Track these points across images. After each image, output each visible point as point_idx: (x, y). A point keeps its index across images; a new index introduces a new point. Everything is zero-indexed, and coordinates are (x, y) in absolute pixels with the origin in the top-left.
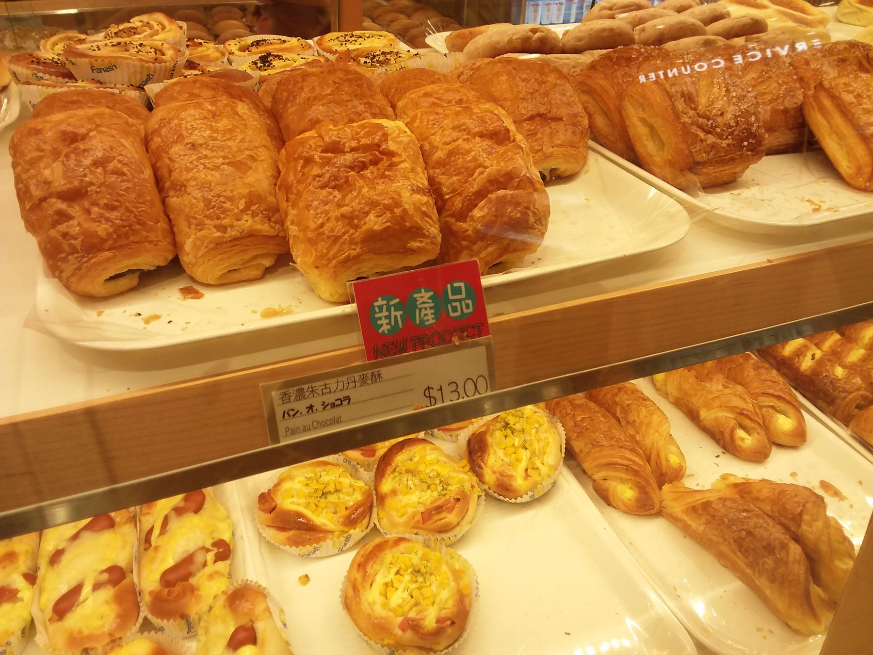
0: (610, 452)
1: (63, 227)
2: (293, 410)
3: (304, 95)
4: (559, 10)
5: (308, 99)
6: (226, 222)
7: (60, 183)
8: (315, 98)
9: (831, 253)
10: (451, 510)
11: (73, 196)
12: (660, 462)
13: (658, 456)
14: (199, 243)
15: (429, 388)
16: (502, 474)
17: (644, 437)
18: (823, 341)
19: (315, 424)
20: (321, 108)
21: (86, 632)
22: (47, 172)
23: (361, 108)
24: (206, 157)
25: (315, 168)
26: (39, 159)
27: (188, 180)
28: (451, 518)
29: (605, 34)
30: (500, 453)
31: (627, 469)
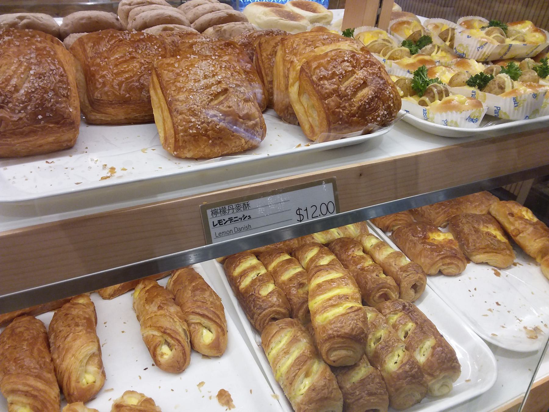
0: (15, 380)
2: (224, 220)
12: (70, 384)
13: (69, 378)
15: (299, 209)
17: (63, 360)
18: (270, 263)
19: (236, 230)
29: (84, 21)
31: (26, 394)
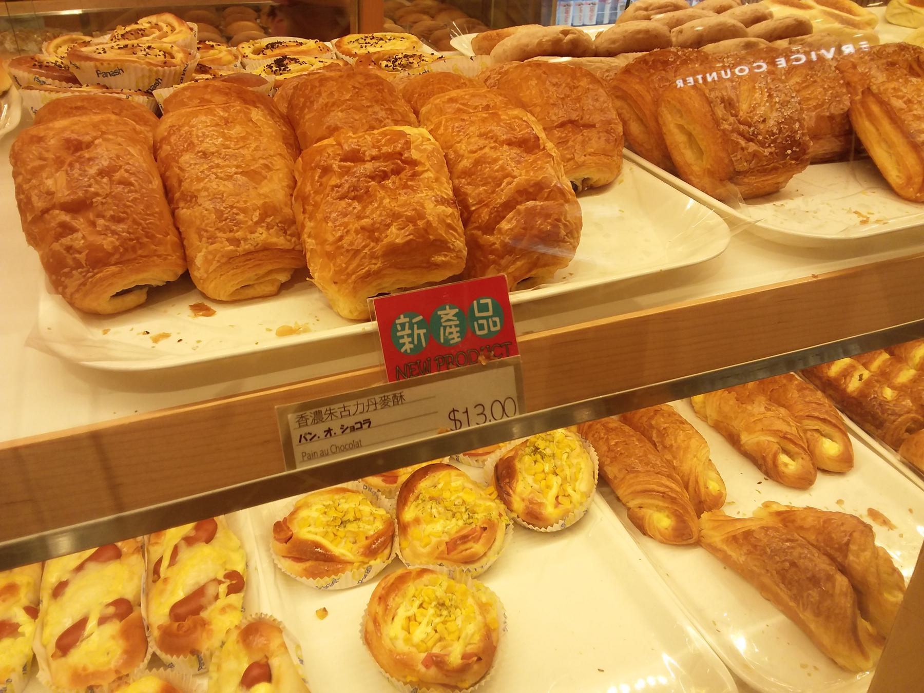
0: (646, 478)
1: (66, 241)
2: (310, 434)
3: (322, 101)
4: (592, 10)
5: (326, 105)
6: (239, 234)
7: (63, 194)
8: (334, 104)
10: (477, 540)
11: (77, 207)
12: (699, 489)
13: (697, 482)
14: (210, 257)
15: (454, 411)
16: (531, 502)
17: (681, 462)
18: (871, 361)
19: (334, 449)
20: (340, 114)
21: (91, 668)
22: (50, 182)
23: (382, 114)
24: (218, 166)
25: (334, 178)
26: (42, 168)
27: (199, 191)
28: (477, 548)
29: (641, 36)
30: (530, 479)
31: (664, 496)
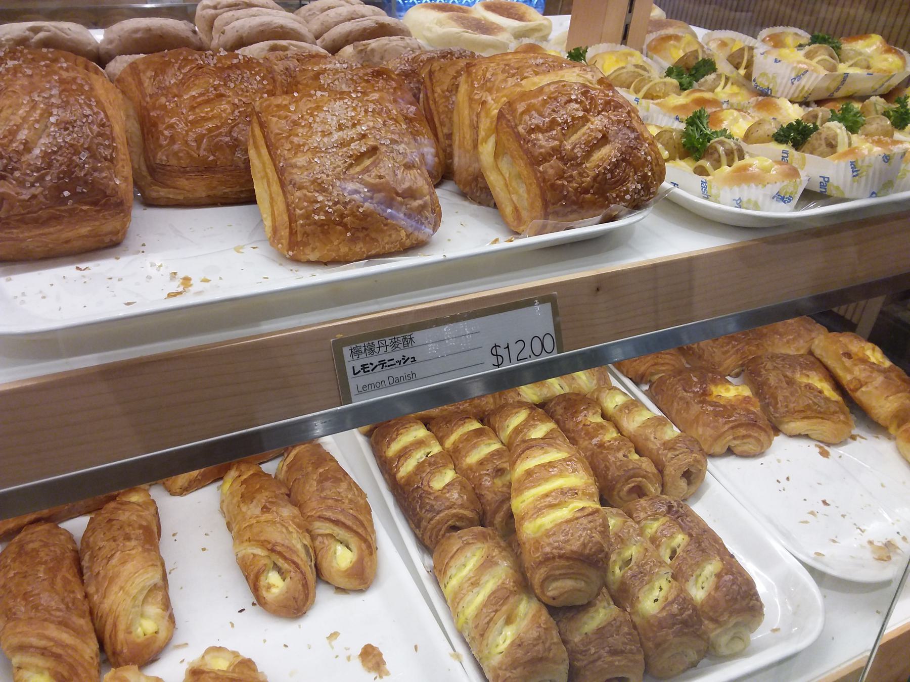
0: (25, 629)
2: (372, 364)
9: (107, 373)
12: (116, 636)
13: (115, 625)
15: (496, 346)
17: (104, 597)
18: (447, 435)
19: (391, 380)
29: (139, 35)
31: (44, 652)
